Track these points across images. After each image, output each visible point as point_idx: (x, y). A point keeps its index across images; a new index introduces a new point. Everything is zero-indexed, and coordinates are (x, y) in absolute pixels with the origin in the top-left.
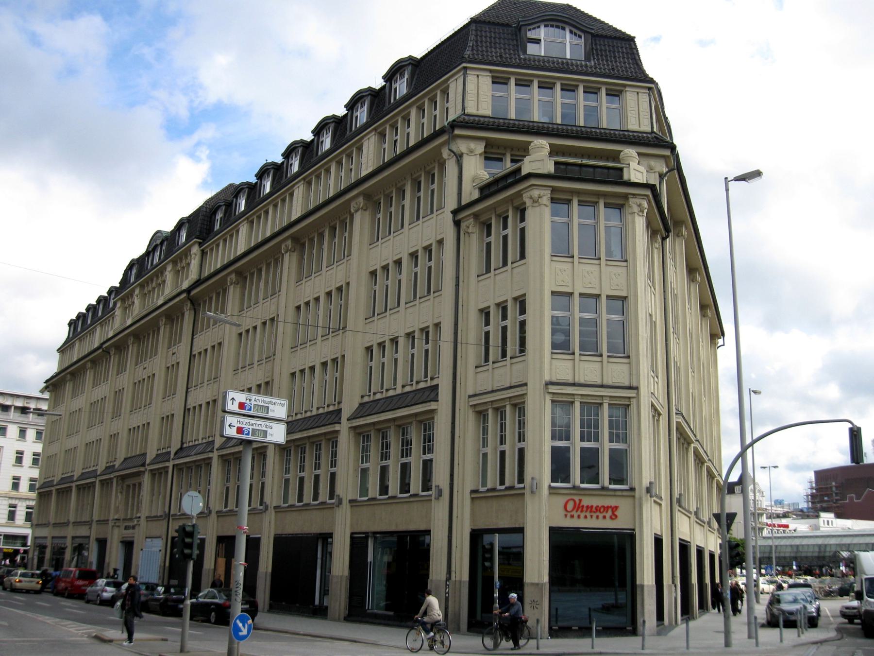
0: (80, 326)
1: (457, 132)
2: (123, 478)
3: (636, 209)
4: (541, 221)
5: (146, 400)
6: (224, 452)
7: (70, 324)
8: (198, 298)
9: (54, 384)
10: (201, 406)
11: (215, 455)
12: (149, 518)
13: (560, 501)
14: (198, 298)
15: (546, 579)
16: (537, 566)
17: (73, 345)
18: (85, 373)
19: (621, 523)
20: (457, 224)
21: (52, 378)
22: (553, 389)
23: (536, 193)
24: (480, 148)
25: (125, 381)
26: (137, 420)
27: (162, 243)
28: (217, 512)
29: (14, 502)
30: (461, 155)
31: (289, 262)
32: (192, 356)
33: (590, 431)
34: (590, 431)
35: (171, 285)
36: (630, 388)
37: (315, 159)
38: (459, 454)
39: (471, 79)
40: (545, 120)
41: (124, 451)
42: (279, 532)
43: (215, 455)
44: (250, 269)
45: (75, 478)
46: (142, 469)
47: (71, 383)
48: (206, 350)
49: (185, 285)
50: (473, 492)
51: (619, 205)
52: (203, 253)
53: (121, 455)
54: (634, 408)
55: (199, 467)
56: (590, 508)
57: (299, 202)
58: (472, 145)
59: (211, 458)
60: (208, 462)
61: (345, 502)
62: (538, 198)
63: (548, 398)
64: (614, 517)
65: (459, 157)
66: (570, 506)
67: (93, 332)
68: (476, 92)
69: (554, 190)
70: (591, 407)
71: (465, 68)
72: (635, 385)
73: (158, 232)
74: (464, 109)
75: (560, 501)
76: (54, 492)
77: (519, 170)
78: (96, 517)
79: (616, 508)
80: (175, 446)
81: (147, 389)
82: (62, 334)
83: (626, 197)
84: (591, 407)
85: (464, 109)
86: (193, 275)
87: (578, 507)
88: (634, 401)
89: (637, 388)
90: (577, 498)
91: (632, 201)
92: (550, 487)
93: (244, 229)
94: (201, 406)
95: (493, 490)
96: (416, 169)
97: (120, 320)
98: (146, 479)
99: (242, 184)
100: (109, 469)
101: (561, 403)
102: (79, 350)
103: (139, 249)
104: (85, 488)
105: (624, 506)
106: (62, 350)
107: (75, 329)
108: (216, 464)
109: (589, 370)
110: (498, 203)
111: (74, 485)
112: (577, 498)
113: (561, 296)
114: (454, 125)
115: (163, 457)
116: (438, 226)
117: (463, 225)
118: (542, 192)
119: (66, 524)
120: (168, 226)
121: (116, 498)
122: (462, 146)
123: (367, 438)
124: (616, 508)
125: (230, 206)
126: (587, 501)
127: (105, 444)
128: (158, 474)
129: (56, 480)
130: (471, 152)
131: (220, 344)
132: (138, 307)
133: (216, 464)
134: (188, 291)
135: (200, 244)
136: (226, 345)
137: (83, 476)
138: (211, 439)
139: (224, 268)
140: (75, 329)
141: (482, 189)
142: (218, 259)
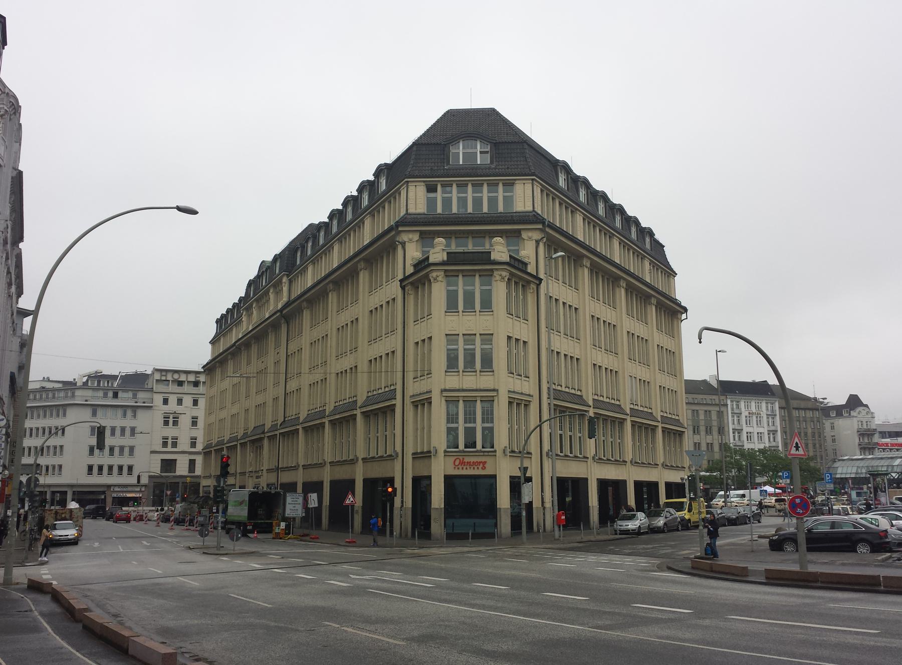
0: (225, 322)
1: (400, 229)
2: (253, 442)
3: (498, 278)
4: (439, 291)
5: (387, 327)
6: (365, 410)
7: (217, 322)
8: (288, 316)
9: (209, 368)
10: (381, 357)
11: (358, 412)
12: (269, 471)
13: (452, 459)
14: (288, 316)
15: (443, 506)
16: (437, 498)
17: (219, 339)
18: (267, 335)
19: (488, 471)
20: (403, 288)
21: (207, 364)
22: (445, 394)
23: (434, 274)
24: (416, 237)
25: (253, 368)
26: (259, 400)
27: (266, 270)
28: (363, 459)
29: (193, 457)
30: (405, 243)
31: (364, 277)
32: (287, 356)
33: (470, 417)
34: (470, 417)
35: (275, 303)
36: (494, 390)
37: (295, 268)
38: (405, 434)
39: (412, 188)
40: (462, 211)
41: (270, 417)
42: (333, 478)
43: (358, 412)
44: (314, 298)
45: (301, 420)
46: (262, 436)
47: (308, 312)
48: (382, 306)
49: (280, 306)
50: (413, 454)
51: (488, 275)
52: (290, 282)
53: (252, 426)
54: (496, 401)
55: (348, 421)
56: (469, 463)
57: (367, 233)
58: (411, 236)
59: (395, 405)
60: (354, 417)
61: (360, 460)
62: (437, 274)
63: (443, 399)
64: (484, 468)
65: (403, 244)
66: (457, 462)
67: (305, 270)
68: (415, 198)
69: (446, 271)
70: (470, 403)
71: (408, 182)
72: (496, 388)
73: (263, 262)
74: (407, 210)
75: (452, 459)
76: (301, 431)
77: (428, 258)
78: (238, 471)
79: (485, 462)
80: (281, 419)
81: (351, 337)
82: (212, 330)
83: (492, 270)
84: (470, 403)
85: (407, 210)
86: (285, 299)
87: (462, 463)
88: (496, 399)
89: (497, 391)
90: (461, 458)
91: (495, 273)
92: (445, 451)
93: (368, 222)
94: (381, 357)
95: (382, 457)
96: (383, 249)
97: (247, 325)
98: (266, 442)
99: (320, 223)
100: (245, 435)
101: (451, 402)
102: (313, 274)
103: (253, 273)
104: (314, 429)
105: (489, 460)
106: (213, 342)
107: (221, 327)
108: (359, 418)
109: (469, 381)
110: (418, 279)
111: (326, 420)
112: (461, 458)
113: (451, 338)
114: (399, 224)
115: (274, 427)
116: (393, 289)
117: (406, 289)
118: (438, 274)
119: (295, 468)
120: (269, 258)
121: (250, 456)
122: (404, 237)
123: (417, 406)
124: (485, 462)
125: (315, 238)
126: (467, 459)
127: (242, 415)
128: (272, 438)
129: (226, 439)
130: (411, 240)
131: (357, 319)
132: (256, 317)
133: (359, 418)
134: (281, 310)
135: (288, 276)
136: (360, 320)
137: (309, 418)
138: (392, 388)
139: (356, 255)
140: (221, 327)
141: (415, 266)
142: (298, 290)
